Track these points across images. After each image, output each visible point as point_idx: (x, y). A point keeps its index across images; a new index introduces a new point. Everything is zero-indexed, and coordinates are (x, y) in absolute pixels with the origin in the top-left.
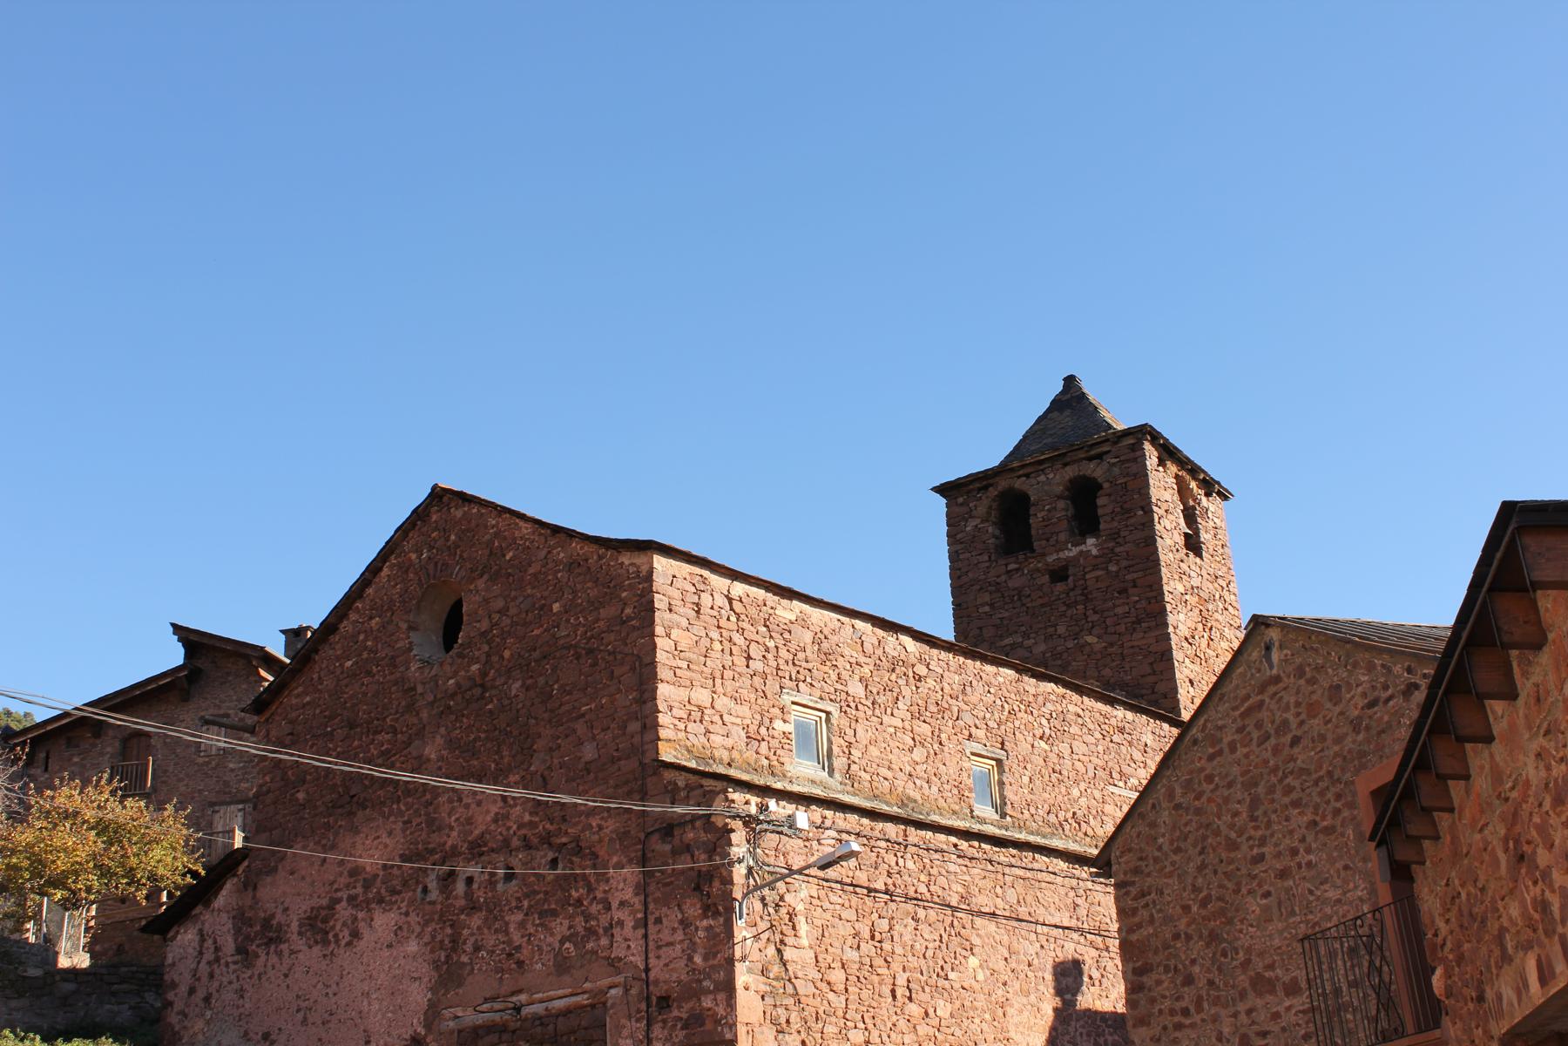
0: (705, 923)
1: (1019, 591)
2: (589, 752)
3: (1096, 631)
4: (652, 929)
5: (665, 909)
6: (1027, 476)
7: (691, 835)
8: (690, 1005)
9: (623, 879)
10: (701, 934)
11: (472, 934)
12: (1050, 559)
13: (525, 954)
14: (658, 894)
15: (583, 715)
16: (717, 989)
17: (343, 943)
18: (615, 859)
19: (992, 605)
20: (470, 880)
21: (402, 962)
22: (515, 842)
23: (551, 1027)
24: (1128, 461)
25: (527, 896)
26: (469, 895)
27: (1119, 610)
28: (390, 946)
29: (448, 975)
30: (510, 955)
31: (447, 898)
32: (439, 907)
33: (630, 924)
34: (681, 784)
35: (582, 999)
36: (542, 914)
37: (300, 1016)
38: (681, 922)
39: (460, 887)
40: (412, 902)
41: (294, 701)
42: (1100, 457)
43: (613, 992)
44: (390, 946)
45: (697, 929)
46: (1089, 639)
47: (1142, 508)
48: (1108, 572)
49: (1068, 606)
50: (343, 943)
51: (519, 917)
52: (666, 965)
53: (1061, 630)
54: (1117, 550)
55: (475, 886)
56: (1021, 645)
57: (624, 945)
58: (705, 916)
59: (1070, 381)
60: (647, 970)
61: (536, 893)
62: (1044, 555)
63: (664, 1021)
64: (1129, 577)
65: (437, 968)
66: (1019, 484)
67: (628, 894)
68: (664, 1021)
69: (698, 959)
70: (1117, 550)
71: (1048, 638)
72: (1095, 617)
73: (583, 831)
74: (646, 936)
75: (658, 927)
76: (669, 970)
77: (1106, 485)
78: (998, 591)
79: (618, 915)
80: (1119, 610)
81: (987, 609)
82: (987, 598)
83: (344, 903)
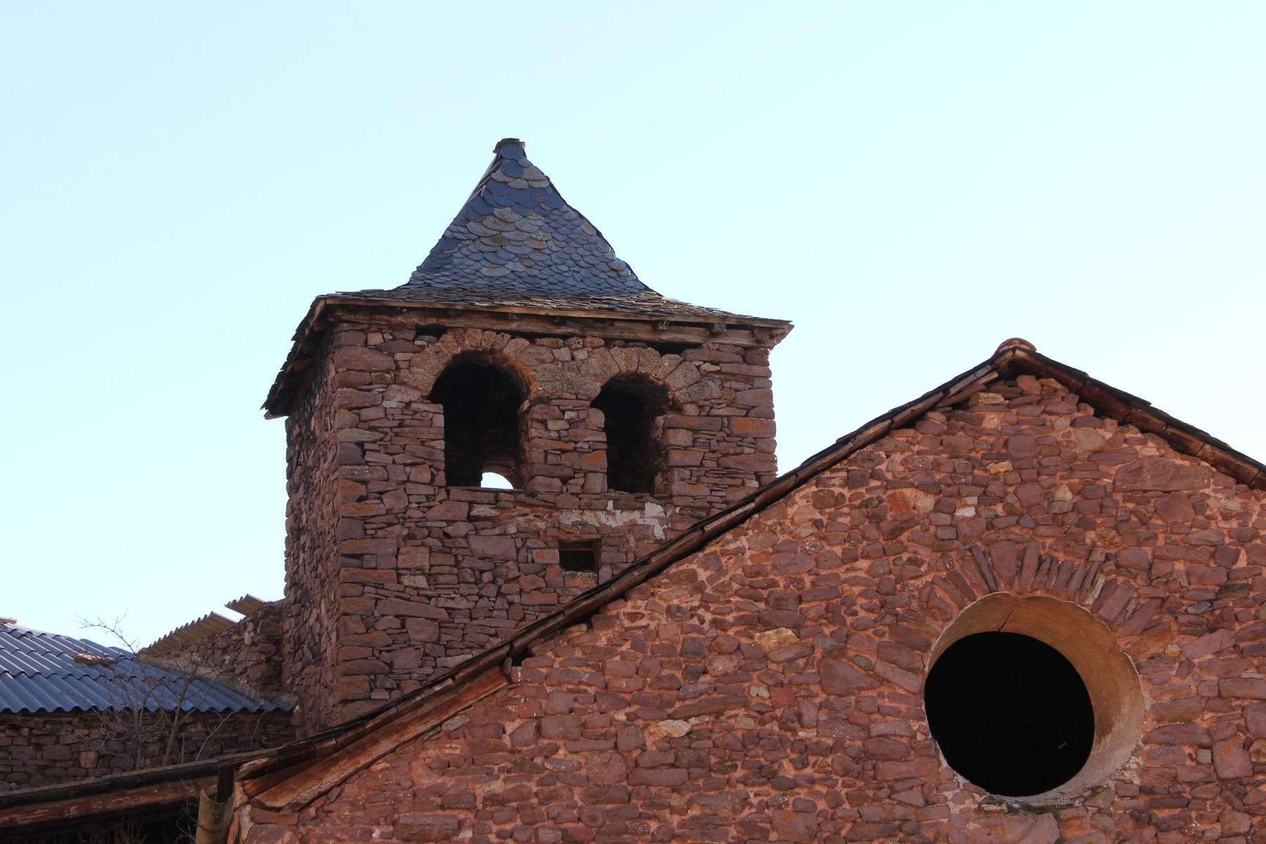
1: (496, 563)
6: (531, 337)
12: (569, 518)
24: (733, 376)
41: (427, 781)
42: (677, 348)
59: (509, 151)
62: (554, 507)
66: (513, 349)
77: (691, 410)
78: (446, 550)
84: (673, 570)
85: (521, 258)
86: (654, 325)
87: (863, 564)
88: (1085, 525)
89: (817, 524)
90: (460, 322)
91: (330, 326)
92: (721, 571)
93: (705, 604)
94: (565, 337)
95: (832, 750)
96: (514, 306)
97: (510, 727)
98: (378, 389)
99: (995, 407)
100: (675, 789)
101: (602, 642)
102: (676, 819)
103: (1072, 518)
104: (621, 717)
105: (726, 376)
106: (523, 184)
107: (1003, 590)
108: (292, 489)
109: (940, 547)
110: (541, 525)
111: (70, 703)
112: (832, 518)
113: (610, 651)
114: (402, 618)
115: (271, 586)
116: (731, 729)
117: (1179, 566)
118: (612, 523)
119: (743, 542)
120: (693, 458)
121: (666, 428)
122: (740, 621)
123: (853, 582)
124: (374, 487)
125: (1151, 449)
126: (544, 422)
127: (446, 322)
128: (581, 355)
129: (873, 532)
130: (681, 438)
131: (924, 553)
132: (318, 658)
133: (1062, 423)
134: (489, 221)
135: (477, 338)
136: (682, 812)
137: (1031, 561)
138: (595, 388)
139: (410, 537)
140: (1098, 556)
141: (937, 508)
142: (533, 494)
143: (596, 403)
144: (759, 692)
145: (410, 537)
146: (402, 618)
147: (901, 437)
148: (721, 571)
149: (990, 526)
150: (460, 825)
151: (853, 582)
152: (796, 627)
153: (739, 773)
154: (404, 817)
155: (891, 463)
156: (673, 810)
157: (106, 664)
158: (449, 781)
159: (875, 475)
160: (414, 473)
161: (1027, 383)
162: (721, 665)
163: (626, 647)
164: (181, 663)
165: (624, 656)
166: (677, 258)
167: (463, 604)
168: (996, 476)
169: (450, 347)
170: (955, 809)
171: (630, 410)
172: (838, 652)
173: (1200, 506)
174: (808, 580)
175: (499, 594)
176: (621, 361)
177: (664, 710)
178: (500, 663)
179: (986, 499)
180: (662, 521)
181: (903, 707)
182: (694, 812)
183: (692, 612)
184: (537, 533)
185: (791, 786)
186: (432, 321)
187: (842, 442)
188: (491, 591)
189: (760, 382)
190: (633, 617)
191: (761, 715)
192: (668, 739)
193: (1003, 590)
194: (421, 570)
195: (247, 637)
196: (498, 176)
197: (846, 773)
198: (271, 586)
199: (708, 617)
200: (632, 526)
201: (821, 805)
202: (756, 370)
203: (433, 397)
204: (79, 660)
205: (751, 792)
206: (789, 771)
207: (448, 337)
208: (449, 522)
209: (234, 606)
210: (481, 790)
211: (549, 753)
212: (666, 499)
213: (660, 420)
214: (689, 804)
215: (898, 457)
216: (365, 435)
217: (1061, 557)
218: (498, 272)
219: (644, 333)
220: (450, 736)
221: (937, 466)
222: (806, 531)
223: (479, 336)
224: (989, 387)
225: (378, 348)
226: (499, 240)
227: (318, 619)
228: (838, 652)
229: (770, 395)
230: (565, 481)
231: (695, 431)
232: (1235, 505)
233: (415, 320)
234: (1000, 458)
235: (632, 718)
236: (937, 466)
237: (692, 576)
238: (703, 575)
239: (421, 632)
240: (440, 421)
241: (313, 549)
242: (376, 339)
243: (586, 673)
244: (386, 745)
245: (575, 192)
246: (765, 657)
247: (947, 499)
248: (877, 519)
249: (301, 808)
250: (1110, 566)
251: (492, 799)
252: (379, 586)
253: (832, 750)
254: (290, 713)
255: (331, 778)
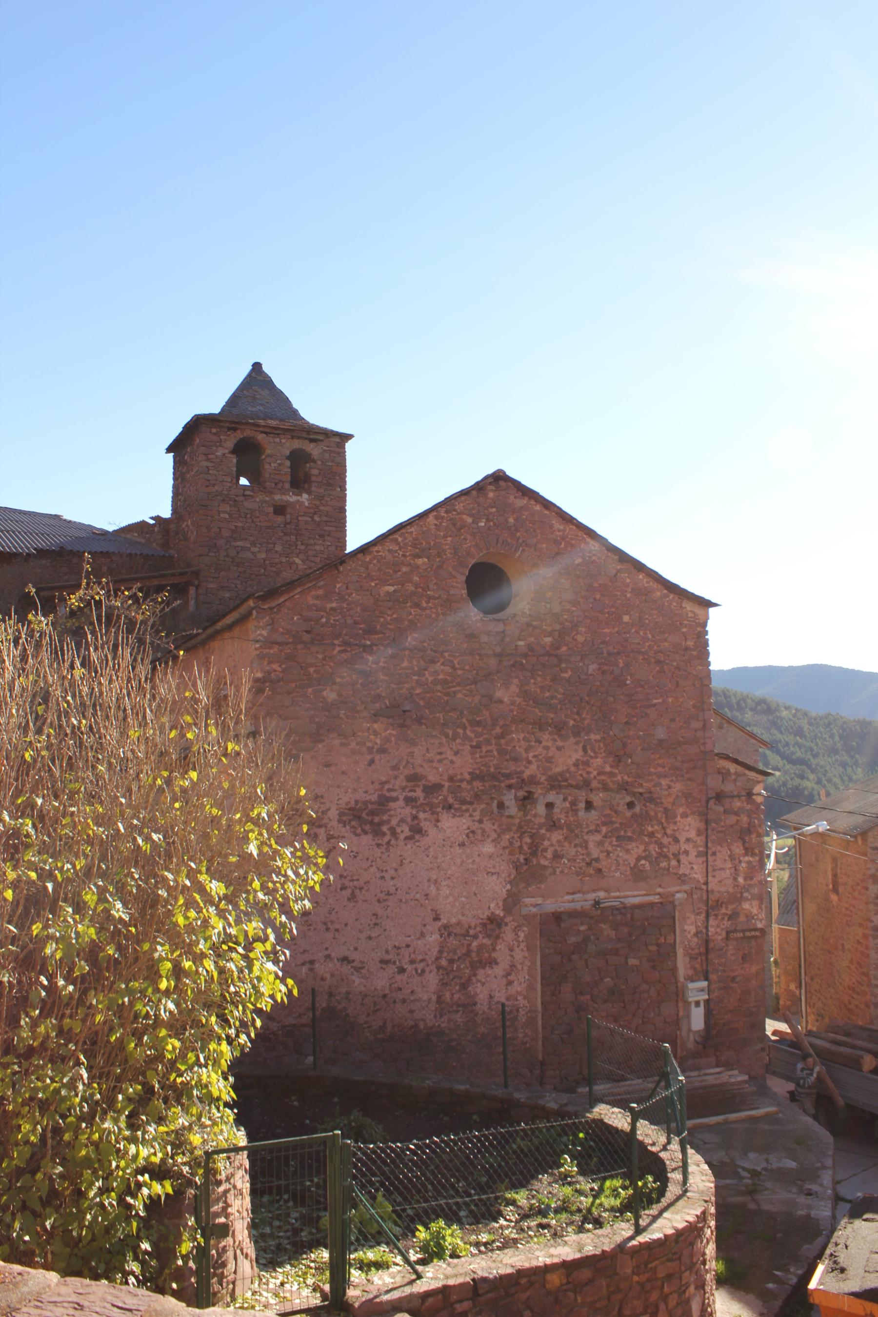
0: (746, 859)
2: (661, 733)
3: (302, 556)
4: (710, 858)
5: (719, 847)
7: (739, 804)
8: (734, 906)
9: (689, 827)
10: (743, 865)
11: (552, 845)
12: (277, 497)
13: (604, 864)
14: (714, 837)
15: (655, 705)
16: (753, 898)
17: (402, 836)
18: (681, 810)
19: (230, 515)
20: (550, 806)
21: (477, 859)
22: (595, 784)
23: (629, 916)
25: (604, 824)
26: (549, 816)
27: (317, 548)
28: (462, 845)
29: (527, 870)
30: (589, 864)
31: (525, 815)
32: (517, 821)
33: (693, 853)
34: (732, 771)
35: (656, 899)
36: (619, 838)
37: (347, 893)
38: (730, 856)
39: (541, 809)
40: (483, 813)
43: (678, 895)
44: (462, 845)
45: (740, 862)
46: (297, 560)
47: (340, 487)
48: (313, 520)
49: (285, 534)
50: (402, 836)
51: (598, 837)
52: (720, 882)
53: (279, 548)
54: (321, 508)
55: (556, 810)
56: (249, 549)
57: (690, 866)
58: (746, 854)
59: (257, 367)
60: (706, 883)
61: (612, 822)
62: (272, 493)
63: (716, 915)
64: (327, 528)
65: (517, 868)
66: (260, 437)
67: (693, 835)
68: (716, 915)
69: (741, 880)
70: (321, 508)
71: (268, 551)
72: (303, 547)
73: (654, 786)
74: (707, 861)
75: (714, 858)
76: (722, 882)
77: (319, 463)
79: (684, 847)
80: (317, 548)
81: (227, 516)
82: (227, 508)
83: (401, 803)
84: (391, 537)
85: (261, 405)
86: (308, 432)
87: (449, 539)
88: (517, 530)
89: (436, 525)
90: (243, 427)
91: (197, 426)
92: (405, 538)
93: (400, 549)
94: (278, 434)
95: (438, 598)
96: (262, 422)
97: (338, 586)
98: (214, 448)
99: (491, 490)
100: (389, 609)
101: (368, 559)
102: (389, 618)
103: (513, 528)
104: (373, 584)
105: (331, 452)
106: (262, 378)
107: (492, 550)
108: (175, 479)
109: (473, 535)
110: (267, 499)
111: (105, 550)
112: (441, 523)
113: (370, 562)
114: (220, 528)
115: (166, 513)
116: (407, 590)
117: (544, 546)
118: (291, 500)
119: (413, 529)
120: (319, 479)
121: (310, 468)
122: (410, 555)
123: (446, 544)
124: (212, 482)
125: (538, 508)
126: (270, 464)
127: (237, 426)
128: (283, 441)
129: (453, 529)
130: (315, 472)
131: (468, 537)
132: (186, 539)
133: (512, 497)
134: (251, 391)
135: (248, 433)
136: (391, 616)
137: (500, 541)
138: (287, 453)
139: (223, 500)
140: (520, 541)
141: (473, 522)
142: (265, 488)
143: (288, 458)
144: (416, 578)
145: (223, 500)
146: (220, 528)
147: (463, 498)
148: (405, 538)
149: (489, 529)
150: (322, 617)
151: (446, 544)
152: (428, 558)
153: (409, 604)
154: (305, 614)
155: (459, 507)
156: (388, 615)
157: (105, 533)
158: (318, 602)
159: (455, 510)
160: (225, 478)
161: (502, 483)
162: (404, 569)
163: (375, 561)
164: (129, 536)
165: (374, 565)
166: (315, 410)
167: (240, 525)
168: (491, 513)
169: (239, 435)
170: (474, 619)
171: (298, 459)
172: (440, 567)
173: (551, 527)
174: (432, 543)
175: (253, 522)
176: (296, 444)
177: (386, 582)
178: (336, 565)
179: (488, 520)
180: (308, 500)
181: (460, 586)
182: (395, 616)
183: (396, 551)
184: (266, 502)
185: (426, 609)
186: (233, 425)
187: (446, 499)
188: (250, 521)
189: (342, 455)
190: (378, 552)
191: (417, 587)
192: (388, 592)
193: (492, 550)
194: (226, 512)
195: (156, 529)
196: (253, 375)
197: (442, 606)
198: (166, 513)
199: (401, 553)
200: (298, 501)
201: (434, 616)
202: (341, 450)
203: (233, 452)
204: (94, 533)
205: (412, 611)
206: (424, 604)
207: (238, 432)
208: (237, 496)
209: (152, 518)
210: (329, 606)
211: (350, 595)
212: (309, 493)
213: (308, 465)
214: (393, 613)
215: (462, 505)
216: (209, 464)
217: (509, 540)
218: (254, 409)
219: (305, 435)
220: (319, 588)
221: (473, 508)
222: (433, 527)
223: (249, 432)
224: (490, 484)
225: (215, 434)
226: (254, 398)
227: (187, 525)
228: (440, 567)
229: (345, 459)
230: (276, 484)
231: (320, 470)
232: (561, 527)
233: (228, 425)
234: (492, 507)
235: (376, 584)
236: (473, 508)
237: (397, 539)
238: (400, 539)
239: (226, 533)
240: (235, 461)
241: (185, 501)
242: (214, 431)
243: (362, 569)
244: (299, 590)
245: (280, 383)
246: (418, 567)
247: (476, 519)
248: (454, 524)
249: (271, 609)
250: (524, 544)
251: (332, 609)
252: (213, 517)
253: (438, 598)
254: (173, 557)
255: (282, 600)
